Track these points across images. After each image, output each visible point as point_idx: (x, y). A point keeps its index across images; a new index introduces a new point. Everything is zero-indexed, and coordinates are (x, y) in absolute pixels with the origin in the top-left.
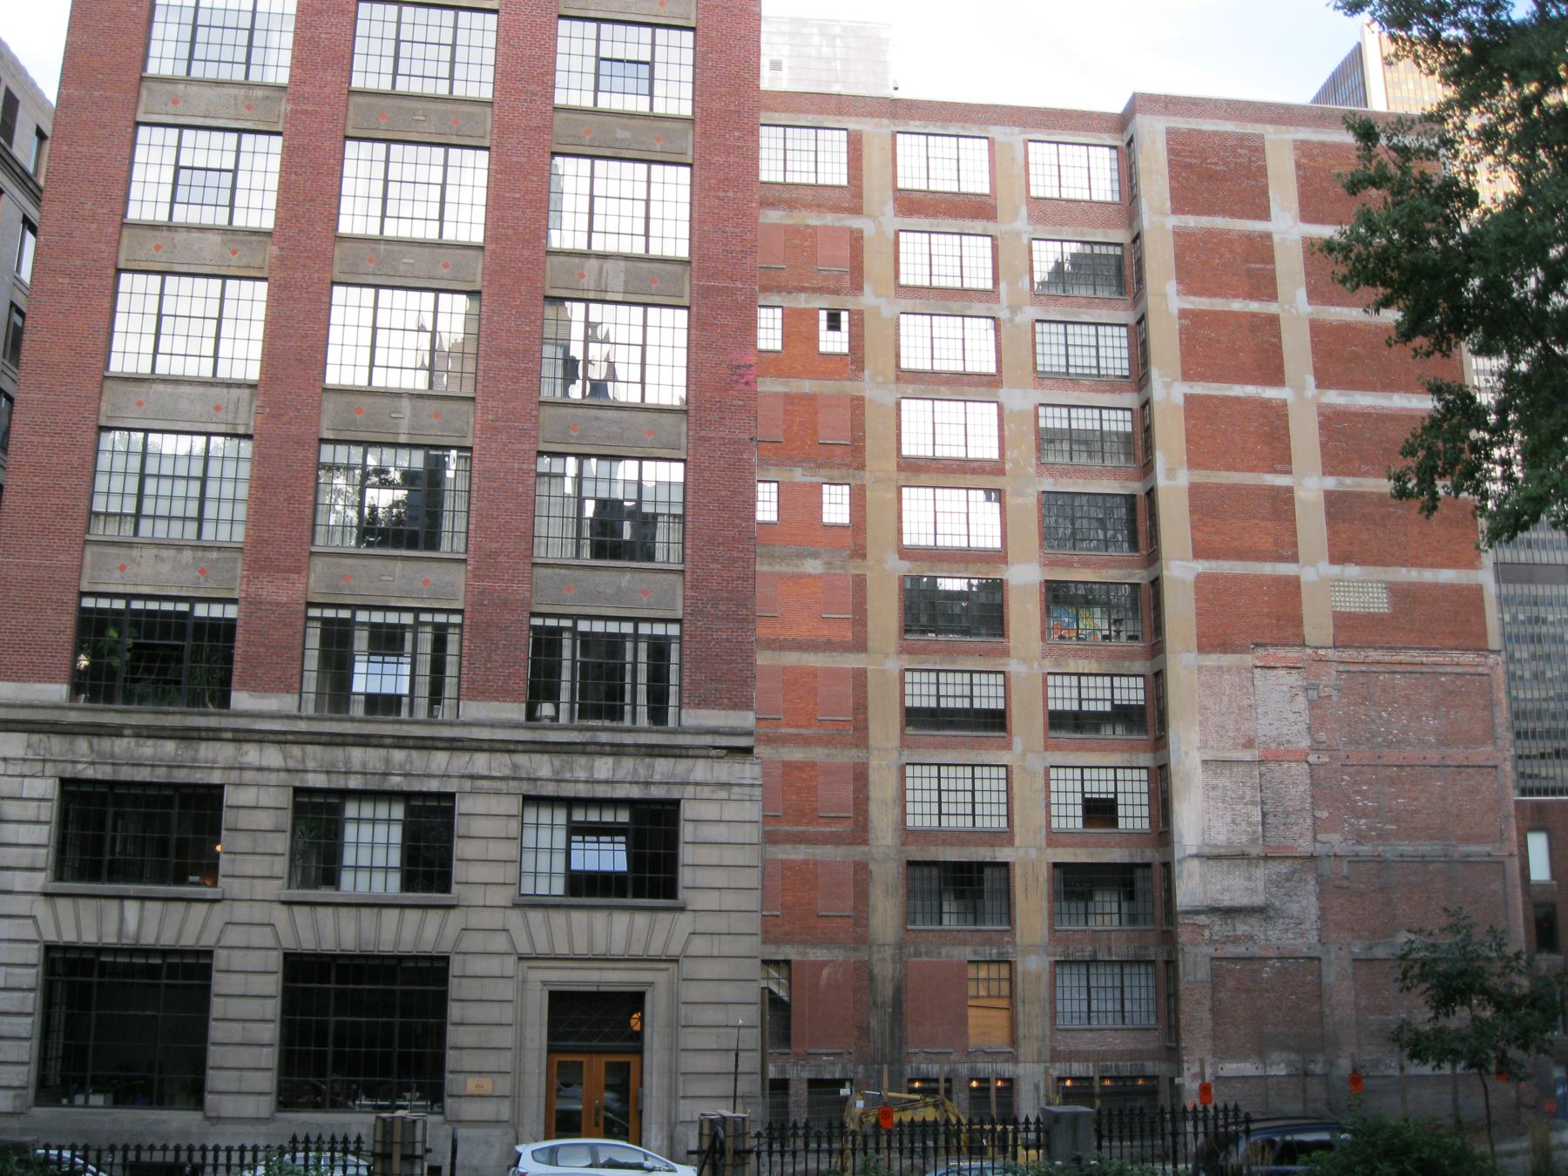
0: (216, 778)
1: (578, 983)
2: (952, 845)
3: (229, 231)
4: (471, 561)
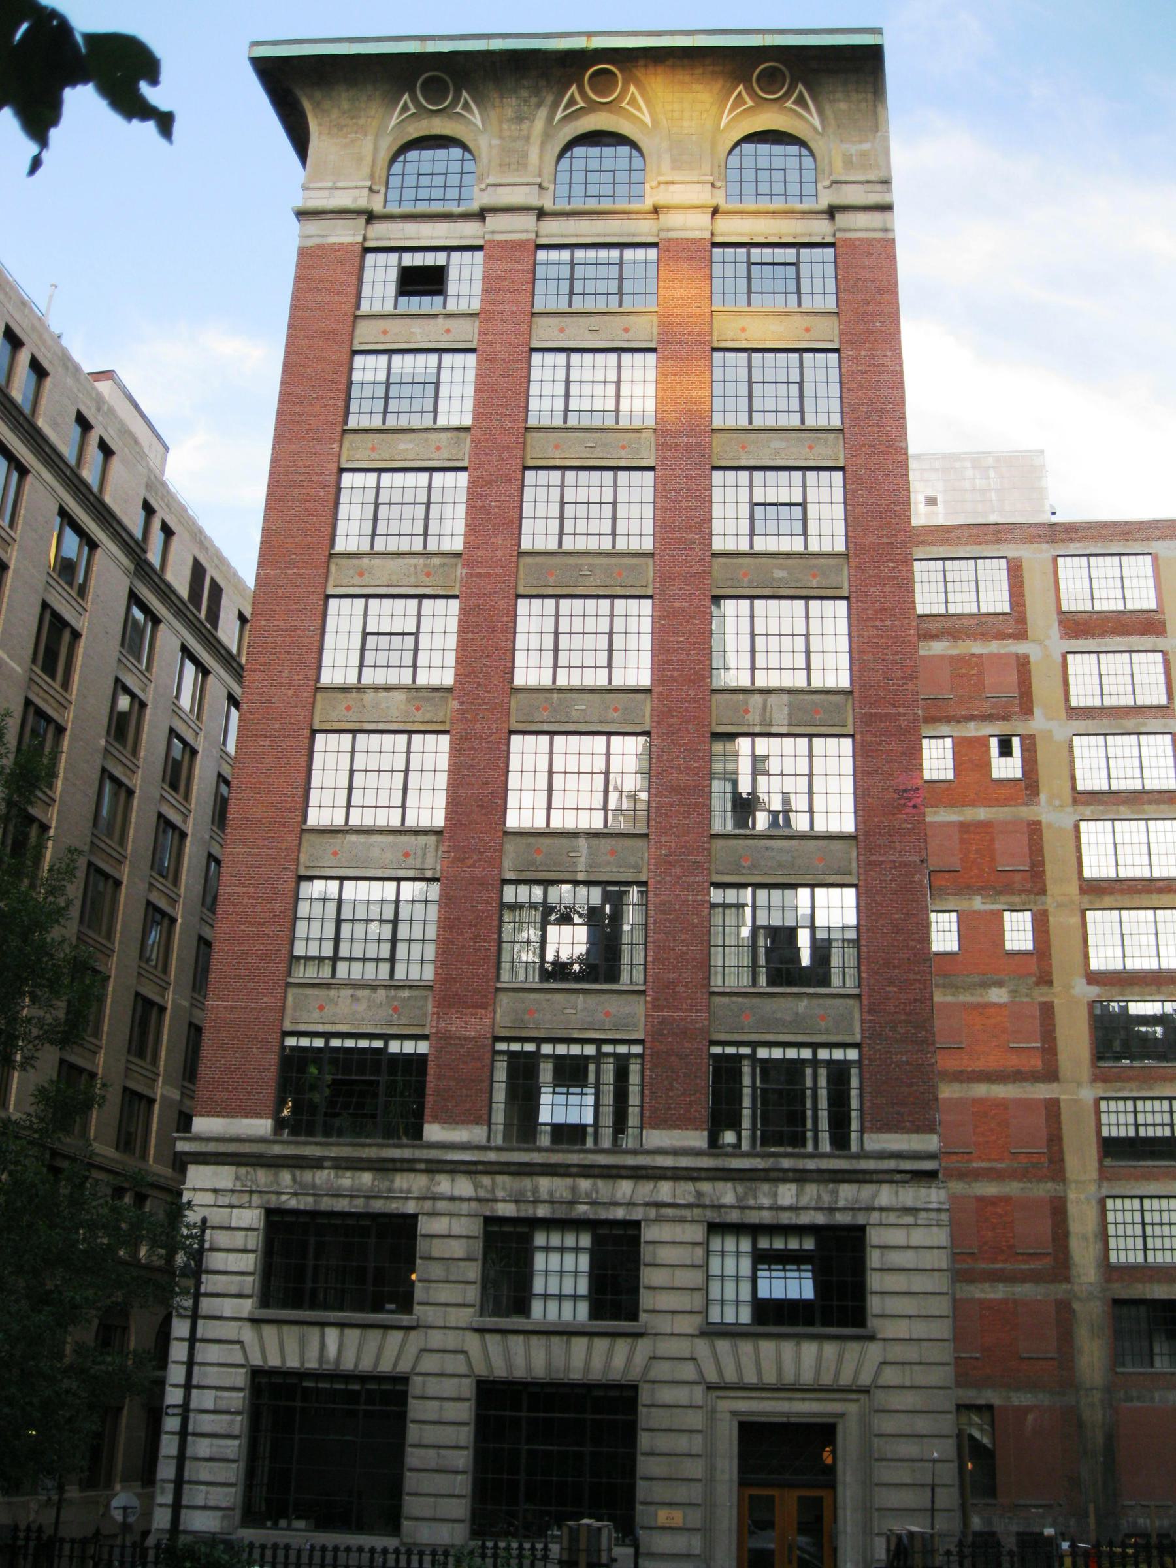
0: (411, 1208)
1: (815, 1414)
2: (1159, 1281)
3: (413, 690)
4: (650, 992)
